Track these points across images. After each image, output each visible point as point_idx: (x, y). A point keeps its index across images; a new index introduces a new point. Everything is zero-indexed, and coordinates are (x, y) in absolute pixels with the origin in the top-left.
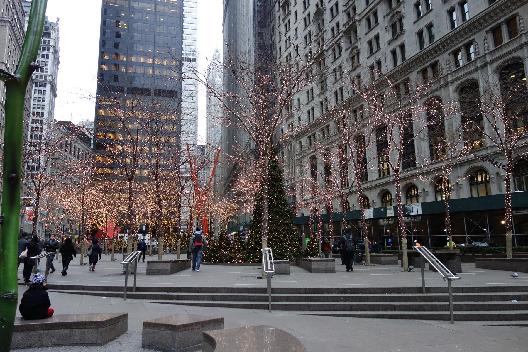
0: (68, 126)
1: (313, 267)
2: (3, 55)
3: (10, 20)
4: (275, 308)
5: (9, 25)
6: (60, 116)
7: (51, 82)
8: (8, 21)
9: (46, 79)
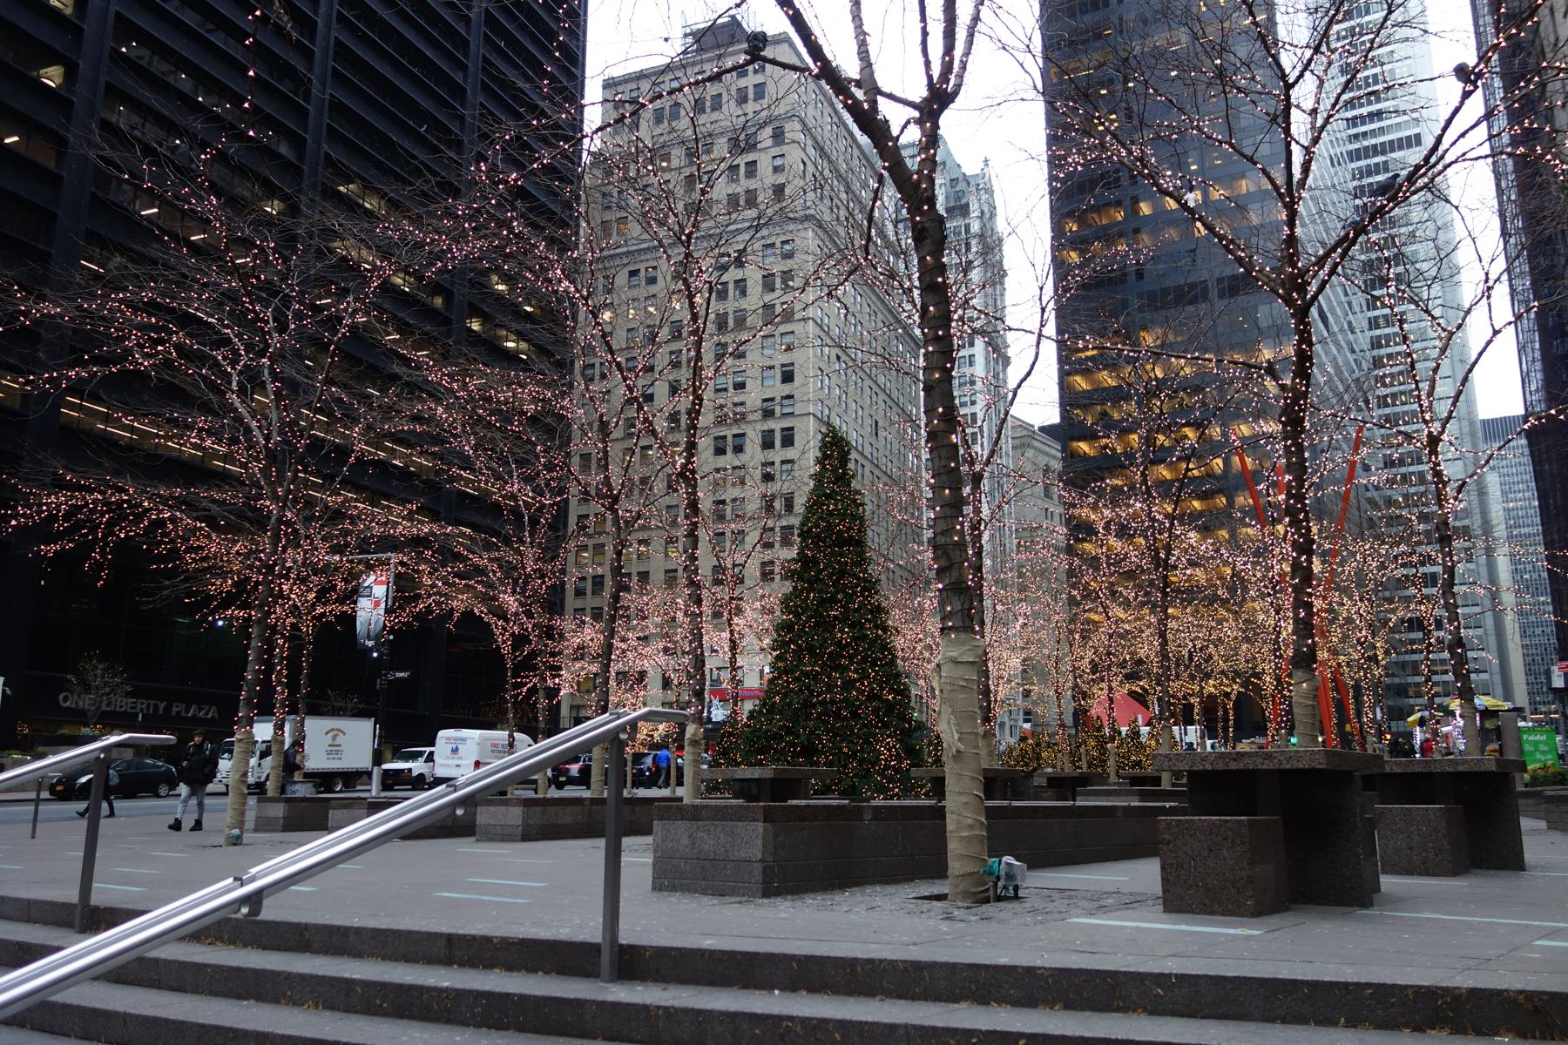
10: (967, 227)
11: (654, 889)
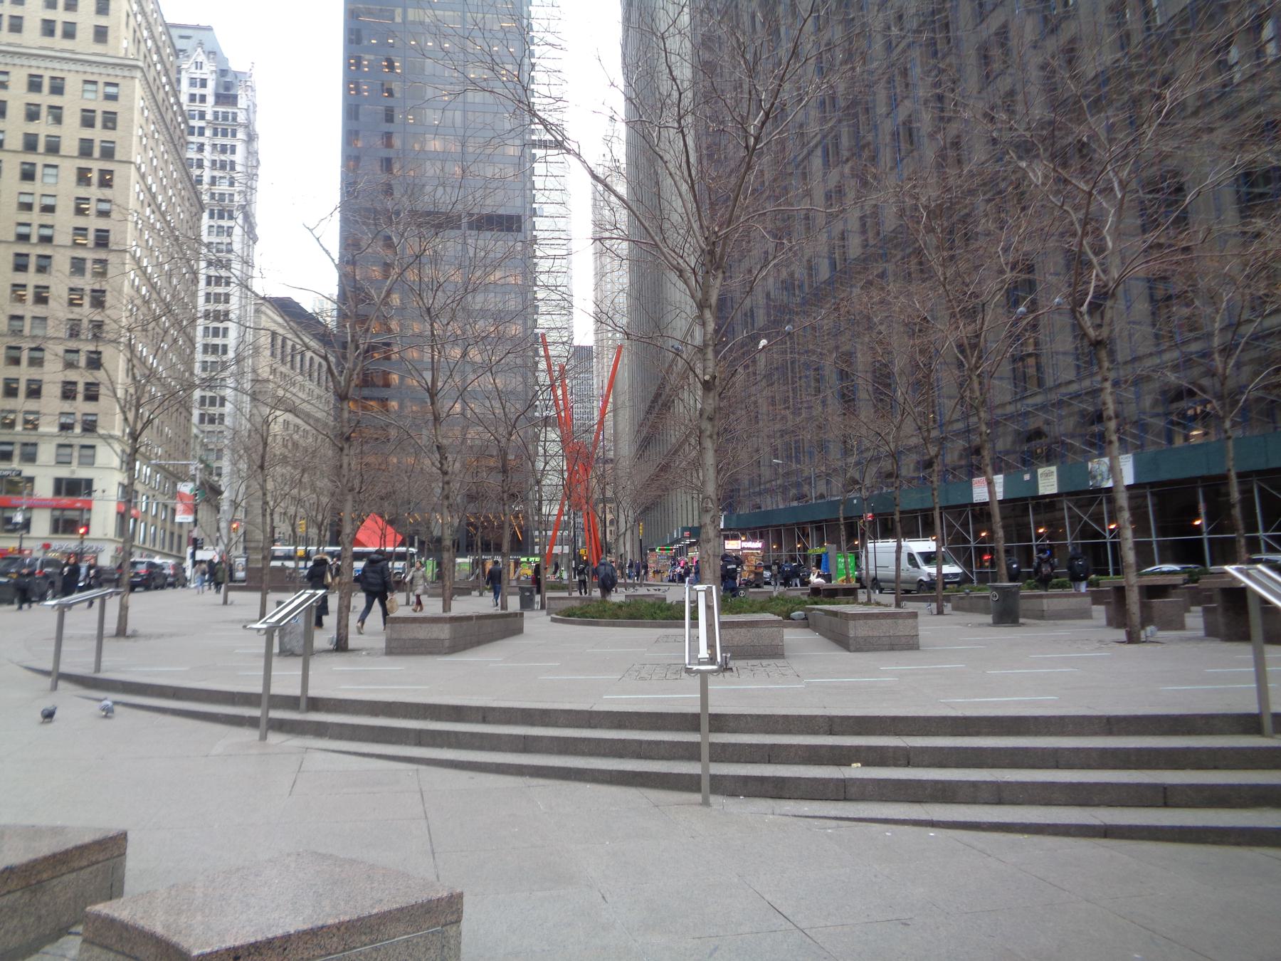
0: (287, 308)
1: (852, 634)
2: (131, 145)
3: (140, 64)
4: (722, 786)
5: (138, 74)
6: (268, 284)
7: (243, 207)
8: (136, 67)
9: (232, 201)
10: (235, 115)
11: (461, 896)
